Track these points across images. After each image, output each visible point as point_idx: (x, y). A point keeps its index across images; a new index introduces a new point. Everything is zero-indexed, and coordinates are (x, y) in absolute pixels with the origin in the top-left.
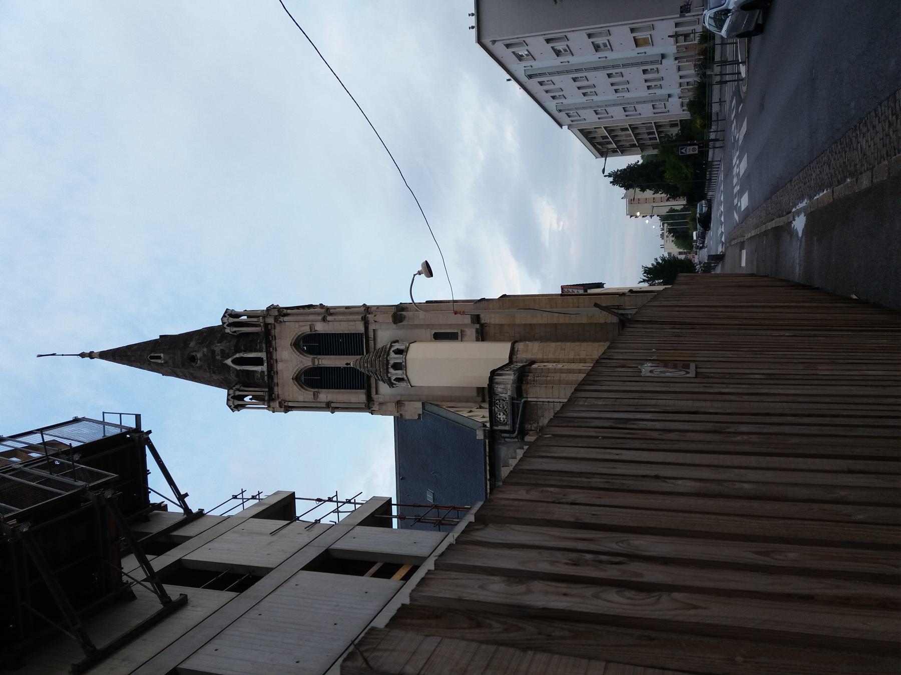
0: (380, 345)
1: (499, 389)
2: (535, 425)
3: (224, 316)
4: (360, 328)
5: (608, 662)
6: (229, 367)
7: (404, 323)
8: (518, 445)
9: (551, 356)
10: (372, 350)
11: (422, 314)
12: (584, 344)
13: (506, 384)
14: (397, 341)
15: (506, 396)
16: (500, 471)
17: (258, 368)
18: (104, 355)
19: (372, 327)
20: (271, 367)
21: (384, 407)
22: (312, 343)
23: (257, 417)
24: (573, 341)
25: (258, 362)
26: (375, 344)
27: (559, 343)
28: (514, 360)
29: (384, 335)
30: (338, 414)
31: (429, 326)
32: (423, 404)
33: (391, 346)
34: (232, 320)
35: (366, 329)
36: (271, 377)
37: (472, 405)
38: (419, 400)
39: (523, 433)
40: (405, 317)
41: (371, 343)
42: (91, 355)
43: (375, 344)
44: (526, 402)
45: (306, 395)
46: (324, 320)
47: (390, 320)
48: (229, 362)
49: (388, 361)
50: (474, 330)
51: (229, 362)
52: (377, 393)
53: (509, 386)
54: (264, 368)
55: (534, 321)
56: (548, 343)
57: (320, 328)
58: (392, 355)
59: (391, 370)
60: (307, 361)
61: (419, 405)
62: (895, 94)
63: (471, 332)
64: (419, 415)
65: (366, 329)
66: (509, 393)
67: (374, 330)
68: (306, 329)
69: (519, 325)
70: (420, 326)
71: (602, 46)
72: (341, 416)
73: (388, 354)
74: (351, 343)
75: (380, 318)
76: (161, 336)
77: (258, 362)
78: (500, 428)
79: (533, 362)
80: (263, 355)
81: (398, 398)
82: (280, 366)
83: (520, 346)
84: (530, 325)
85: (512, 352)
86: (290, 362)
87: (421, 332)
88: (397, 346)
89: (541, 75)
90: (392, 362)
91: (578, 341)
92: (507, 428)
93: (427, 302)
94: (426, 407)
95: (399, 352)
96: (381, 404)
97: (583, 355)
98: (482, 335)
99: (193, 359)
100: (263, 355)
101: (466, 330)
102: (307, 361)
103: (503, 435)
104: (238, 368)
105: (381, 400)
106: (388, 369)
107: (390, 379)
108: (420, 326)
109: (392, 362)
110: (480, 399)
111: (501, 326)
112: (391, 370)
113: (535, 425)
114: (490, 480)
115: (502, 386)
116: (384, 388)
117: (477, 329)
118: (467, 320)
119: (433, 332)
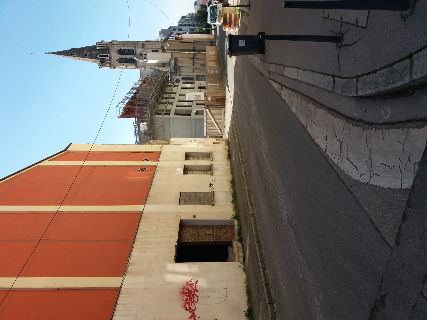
5: (282, 86)
9: (180, 57)
13: (173, 62)
18: (54, 53)
19: (136, 48)
22: (120, 52)
23: (107, 70)
25: (107, 56)
29: (139, 51)
42: (46, 53)
46: (124, 46)
48: (98, 56)
51: (98, 56)
54: (108, 58)
57: (123, 48)
60: (120, 56)
62: (421, 293)
63: (161, 50)
68: (119, 48)
70: (149, 48)
74: (132, 52)
82: (112, 57)
85: (172, 56)
86: (115, 56)
87: (149, 50)
93: (146, 41)
95: (145, 55)
98: (164, 51)
99: (86, 55)
100: (108, 55)
102: (120, 56)
104: (101, 58)
108: (149, 48)
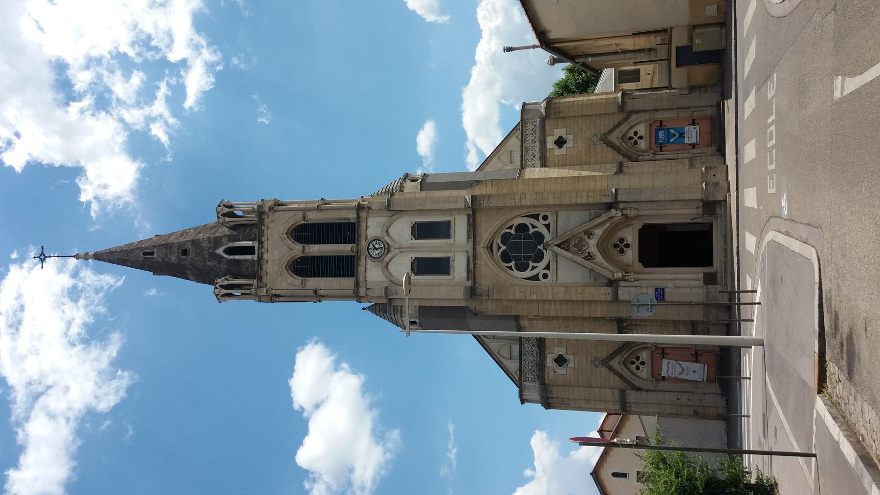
3: (219, 206)
4: (352, 216)
6: (222, 257)
17: (249, 257)
20: (260, 258)
22: (305, 232)
25: (250, 250)
30: (325, 303)
34: (227, 210)
36: (260, 266)
45: (293, 282)
48: (220, 251)
51: (220, 251)
60: (297, 250)
63: (523, 340)
64: (658, 430)
71: (582, 235)
77: (250, 250)
80: (256, 244)
86: (278, 250)
89: (586, 56)
102: (297, 250)
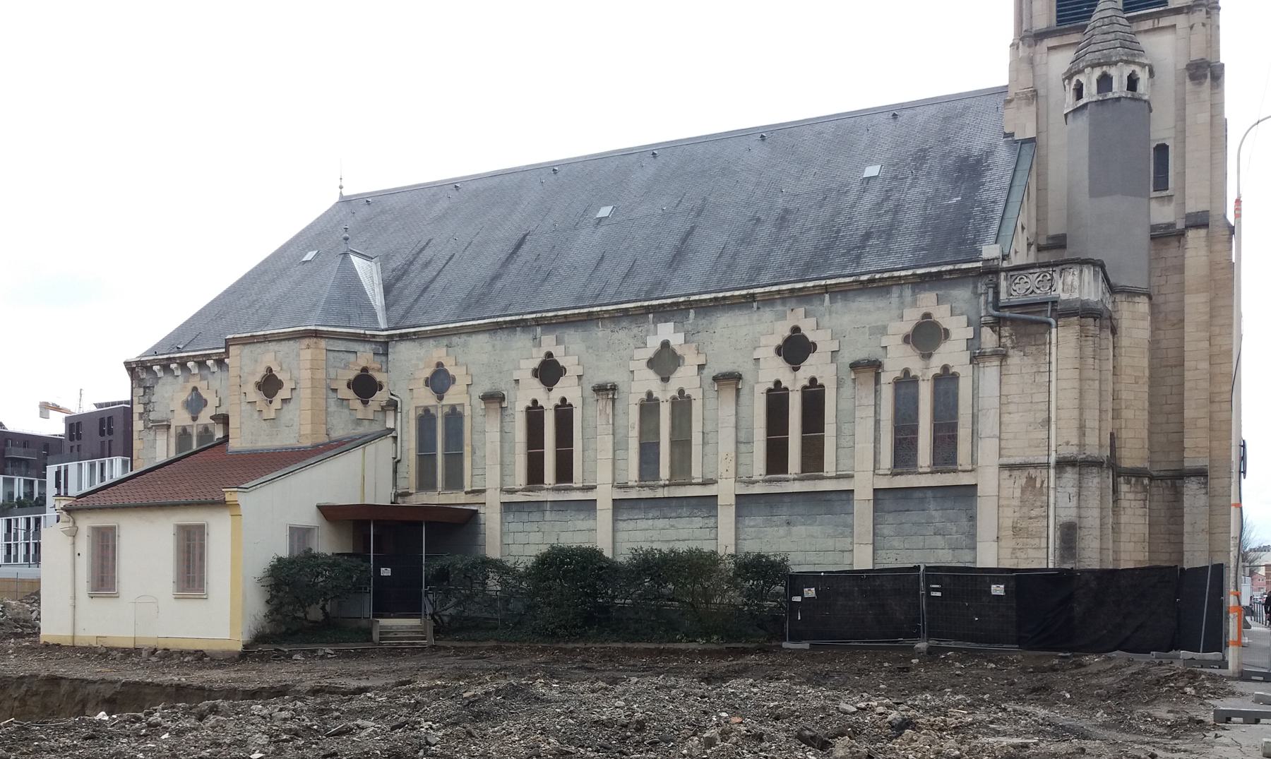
0: (1145, 41)
1: (1072, 277)
2: (1009, 343)
7: (1189, 85)
8: (974, 318)
9: (1124, 361)
10: (1135, 27)
11: (1204, 117)
12: (1146, 415)
14: (1151, 73)
15: (1059, 291)
16: (931, 289)
19: (1181, 20)
21: (1025, 66)
24: (1151, 396)
26: (1146, 31)
27: (1147, 373)
28: (1118, 297)
31: (1181, 133)
32: (1032, 140)
33: (1143, 66)
35: (1178, 11)
37: (1033, 230)
38: (1038, 133)
39: (997, 324)
40: (1201, 84)
41: (1148, 24)
43: (1146, 31)
44: (1049, 324)
47: (1195, 56)
49: (1116, 63)
50: (1171, 220)
52: (1049, 49)
53: (1076, 295)
55: (1189, 329)
56: (1147, 354)
58: (1127, 70)
59: (1097, 72)
61: (1030, 133)
64: (1012, 135)
65: (1178, 11)
66: (1064, 296)
67: (1174, 26)
69: (1182, 301)
72: (1243, 423)
73: (1127, 62)
75: (1199, 36)
76: (1223, 65)
78: (1003, 284)
79: (1114, 331)
81: (1041, 92)
83: (1143, 305)
84: (1182, 321)
88: (1143, 75)
90: (1113, 71)
91: (1151, 404)
92: (1003, 296)
94: (1026, 147)
96: (1031, 61)
97: (1127, 414)
101: (1173, 205)
103: (991, 291)
105: (1038, 58)
106: (1100, 65)
107: (1080, 71)
109: (1113, 71)
110: (1043, 242)
111: (1181, 269)
112: (1097, 72)
113: (1009, 343)
114: (914, 275)
115: (1076, 283)
116: (1060, 62)
117: (1172, 225)
118: (1192, 207)
119: (1169, 143)
